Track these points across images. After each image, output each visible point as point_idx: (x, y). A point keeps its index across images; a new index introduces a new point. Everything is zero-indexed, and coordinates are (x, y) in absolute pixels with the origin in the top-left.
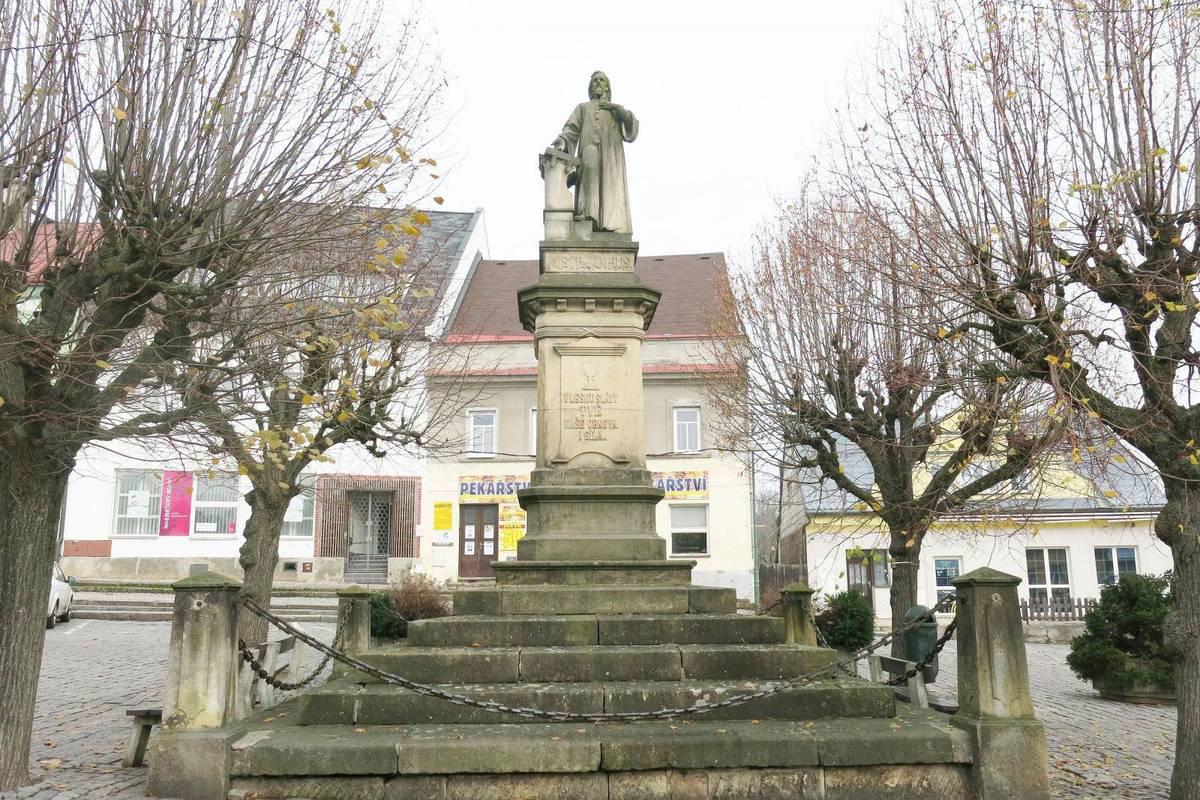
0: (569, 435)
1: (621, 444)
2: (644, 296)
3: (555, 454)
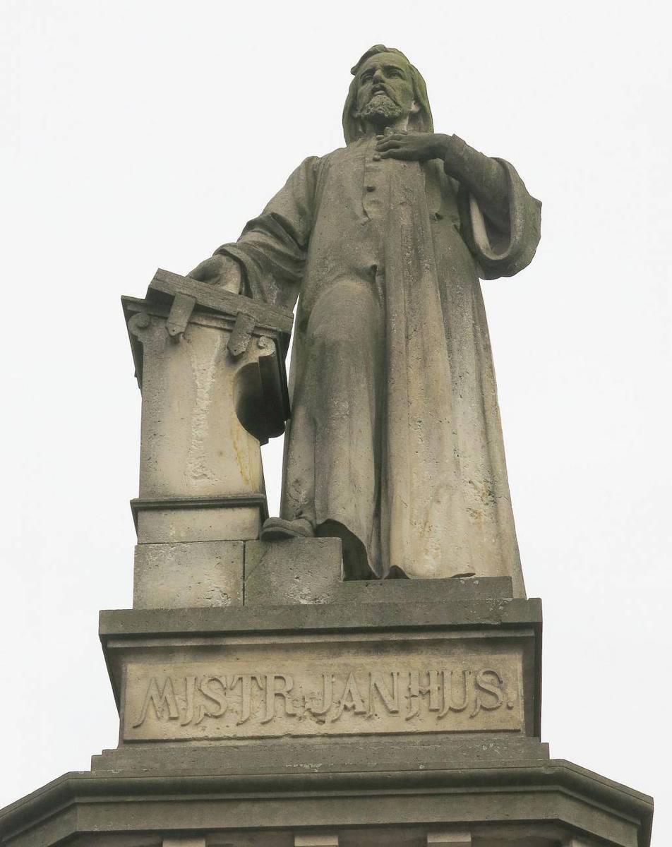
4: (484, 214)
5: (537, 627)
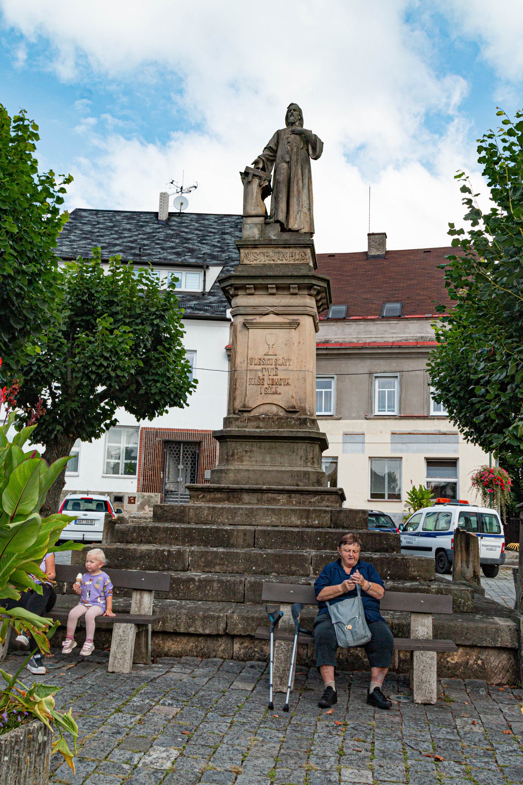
0: (251, 390)
1: (293, 397)
2: (314, 282)
3: (241, 405)
4: (312, 146)
5: (313, 245)
